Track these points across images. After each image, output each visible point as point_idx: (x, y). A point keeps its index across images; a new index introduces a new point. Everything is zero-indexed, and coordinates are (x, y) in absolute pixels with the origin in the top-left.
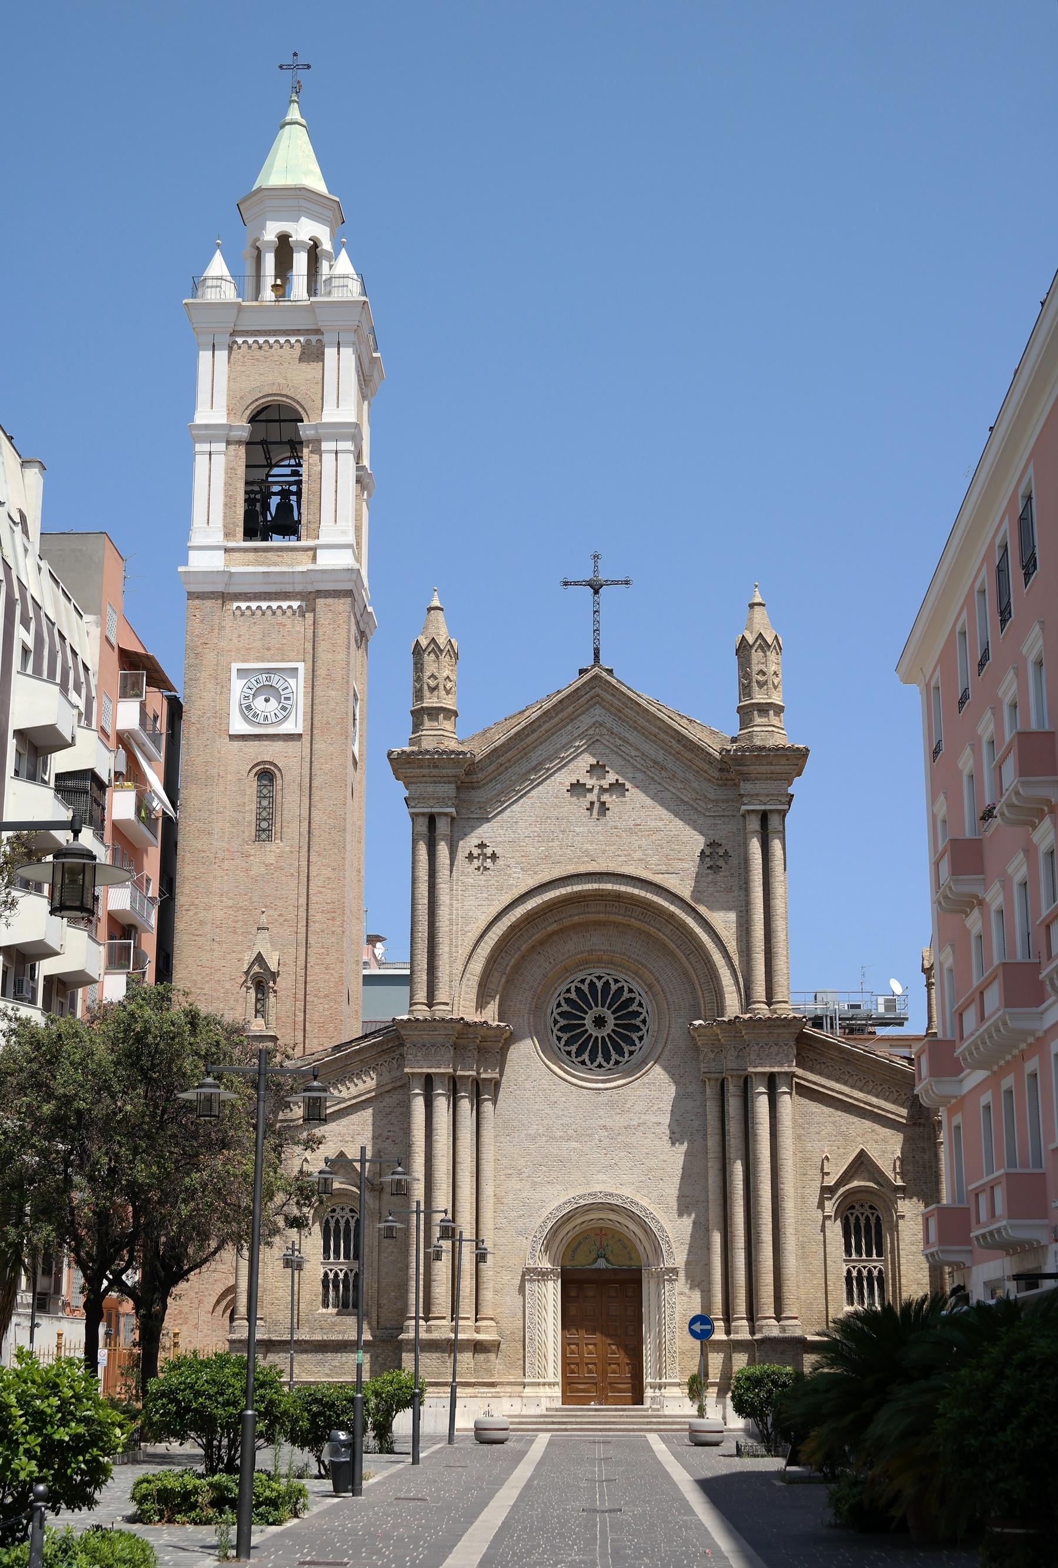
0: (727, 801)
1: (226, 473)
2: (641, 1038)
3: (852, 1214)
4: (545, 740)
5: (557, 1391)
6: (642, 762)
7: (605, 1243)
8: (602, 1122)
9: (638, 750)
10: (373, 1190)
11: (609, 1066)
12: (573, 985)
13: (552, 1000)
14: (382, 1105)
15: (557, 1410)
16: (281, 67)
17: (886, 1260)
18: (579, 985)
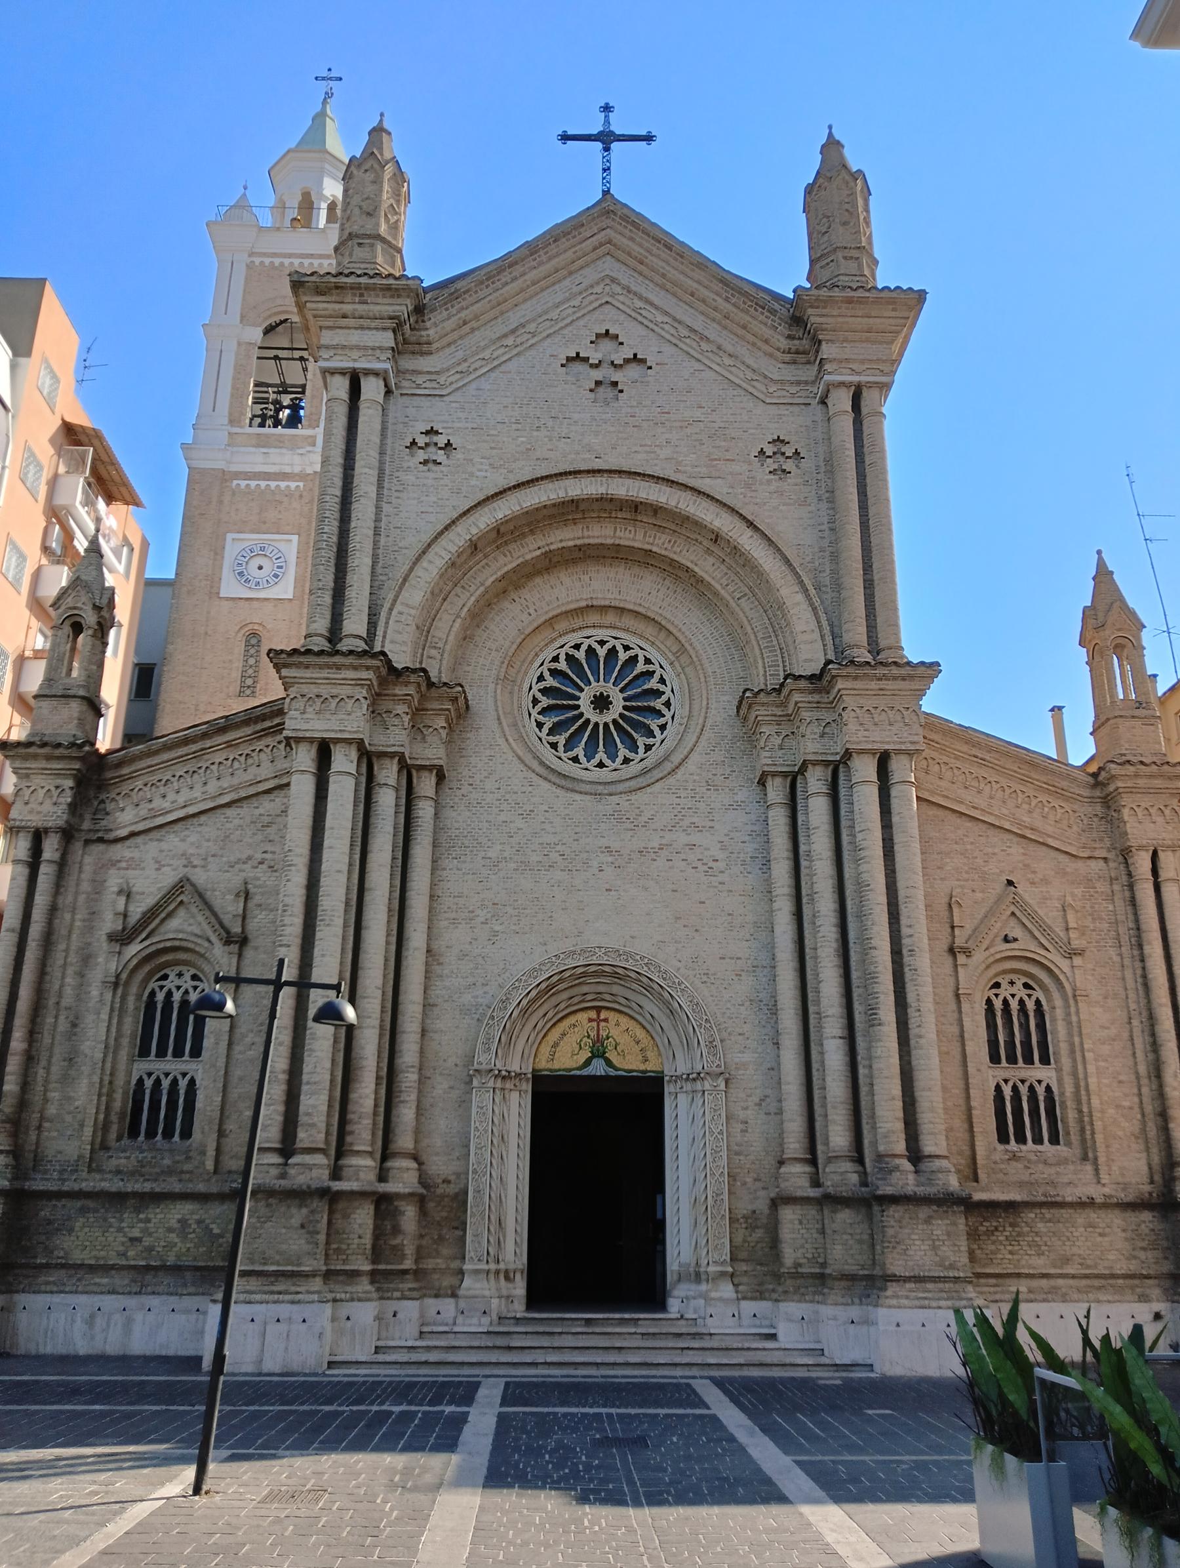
0: (798, 383)
1: (235, 369)
2: (663, 728)
3: (997, 995)
4: (531, 297)
5: (519, 1288)
6: (673, 331)
7: (604, 1034)
8: (604, 842)
9: (666, 313)
10: (228, 942)
11: (614, 766)
12: (562, 652)
13: (531, 672)
14: (257, 812)
15: (518, 1321)
16: (316, 78)
17: (1059, 1070)
18: (572, 652)
